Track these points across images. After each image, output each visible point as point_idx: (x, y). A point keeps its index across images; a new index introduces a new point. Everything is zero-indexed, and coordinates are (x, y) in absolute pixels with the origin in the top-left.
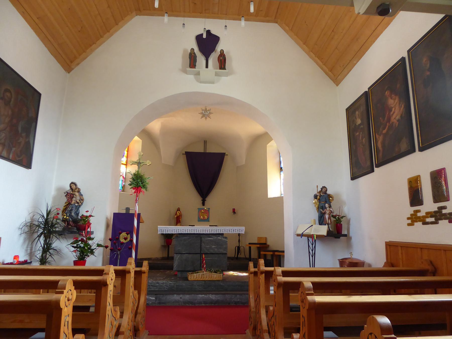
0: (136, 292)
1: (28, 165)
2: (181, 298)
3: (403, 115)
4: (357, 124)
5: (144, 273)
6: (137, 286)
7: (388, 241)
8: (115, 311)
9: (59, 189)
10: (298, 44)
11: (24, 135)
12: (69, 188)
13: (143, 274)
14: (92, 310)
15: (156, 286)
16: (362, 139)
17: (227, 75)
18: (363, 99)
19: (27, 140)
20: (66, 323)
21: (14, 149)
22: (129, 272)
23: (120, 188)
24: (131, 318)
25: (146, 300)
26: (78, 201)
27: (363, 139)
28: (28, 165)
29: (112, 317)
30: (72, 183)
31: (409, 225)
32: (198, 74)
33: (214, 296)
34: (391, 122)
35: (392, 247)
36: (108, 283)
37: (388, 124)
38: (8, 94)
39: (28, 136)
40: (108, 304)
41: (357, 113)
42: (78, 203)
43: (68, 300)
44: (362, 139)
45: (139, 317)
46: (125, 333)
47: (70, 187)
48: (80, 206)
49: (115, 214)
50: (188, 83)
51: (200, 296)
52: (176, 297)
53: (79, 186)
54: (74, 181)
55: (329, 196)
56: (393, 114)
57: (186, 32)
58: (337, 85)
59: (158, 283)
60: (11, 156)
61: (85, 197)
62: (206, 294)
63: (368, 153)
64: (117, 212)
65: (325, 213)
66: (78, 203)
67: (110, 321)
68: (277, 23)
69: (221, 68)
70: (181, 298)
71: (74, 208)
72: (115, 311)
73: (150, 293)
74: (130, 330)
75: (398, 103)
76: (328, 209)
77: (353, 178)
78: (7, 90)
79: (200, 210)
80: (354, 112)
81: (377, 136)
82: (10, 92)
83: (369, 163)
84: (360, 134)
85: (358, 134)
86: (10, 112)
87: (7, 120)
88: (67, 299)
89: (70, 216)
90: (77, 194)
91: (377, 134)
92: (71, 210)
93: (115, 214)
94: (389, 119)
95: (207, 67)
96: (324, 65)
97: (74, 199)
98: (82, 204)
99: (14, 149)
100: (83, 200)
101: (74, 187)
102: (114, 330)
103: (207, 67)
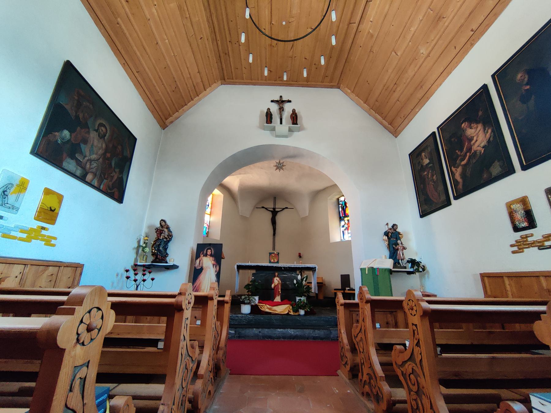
0: (219, 323)
1: (120, 199)
2: (260, 332)
3: (491, 139)
4: (425, 164)
5: (227, 303)
6: (219, 317)
7: (482, 272)
8: (192, 347)
9: (150, 227)
10: (358, 104)
11: (117, 170)
12: (159, 225)
13: (225, 304)
14: (161, 345)
15: (236, 320)
16: (432, 176)
17: (300, 130)
18: (432, 139)
19: (120, 176)
20: (77, 382)
21: (105, 181)
22: (212, 299)
23: (204, 233)
24: (212, 355)
25: (228, 333)
26: (166, 236)
27: (433, 176)
28: (120, 199)
29: (188, 358)
30: (162, 220)
31: (514, 252)
32: (273, 129)
33: (292, 330)
34: (473, 151)
35: (491, 280)
36: (184, 307)
37: (468, 154)
38: (103, 129)
39: (121, 172)
40: (182, 337)
41: (423, 154)
42: (166, 238)
43: (89, 329)
44: (432, 176)
45: (221, 353)
46: (204, 376)
47: (160, 224)
48: (169, 241)
49: (198, 245)
50: (264, 138)
51: (279, 330)
52: (255, 331)
53: (168, 223)
54: (164, 219)
55: (399, 233)
56: (474, 144)
57: (262, 97)
58: (396, 137)
59: (238, 317)
60: (102, 187)
61: (174, 234)
62: (285, 329)
63: (441, 188)
64: (202, 243)
65: (398, 249)
66: (166, 238)
67: (183, 365)
68: (339, 88)
69: (293, 124)
70: (260, 332)
71: (162, 243)
72: (192, 347)
73: (231, 326)
74: (211, 372)
75: (482, 130)
76: (400, 245)
77: (422, 216)
78: (101, 125)
79: (270, 254)
80: (419, 154)
81: (453, 169)
82: (104, 126)
83: (443, 198)
84: (428, 173)
85: (425, 173)
86: (104, 146)
87: (101, 152)
88: (83, 327)
89: (159, 250)
90: (166, 230)
91: (453, 168)
92: (160, 245)
93: (198, 245)
94: (470, 149)
95: (281, 123)
96: (384, 119)
97: (163, 234)
98: (170, 239)
99: (105, 181)
100: (171, 236)
101: (163, 224)
102: (191, 375)
103: (281, 123)
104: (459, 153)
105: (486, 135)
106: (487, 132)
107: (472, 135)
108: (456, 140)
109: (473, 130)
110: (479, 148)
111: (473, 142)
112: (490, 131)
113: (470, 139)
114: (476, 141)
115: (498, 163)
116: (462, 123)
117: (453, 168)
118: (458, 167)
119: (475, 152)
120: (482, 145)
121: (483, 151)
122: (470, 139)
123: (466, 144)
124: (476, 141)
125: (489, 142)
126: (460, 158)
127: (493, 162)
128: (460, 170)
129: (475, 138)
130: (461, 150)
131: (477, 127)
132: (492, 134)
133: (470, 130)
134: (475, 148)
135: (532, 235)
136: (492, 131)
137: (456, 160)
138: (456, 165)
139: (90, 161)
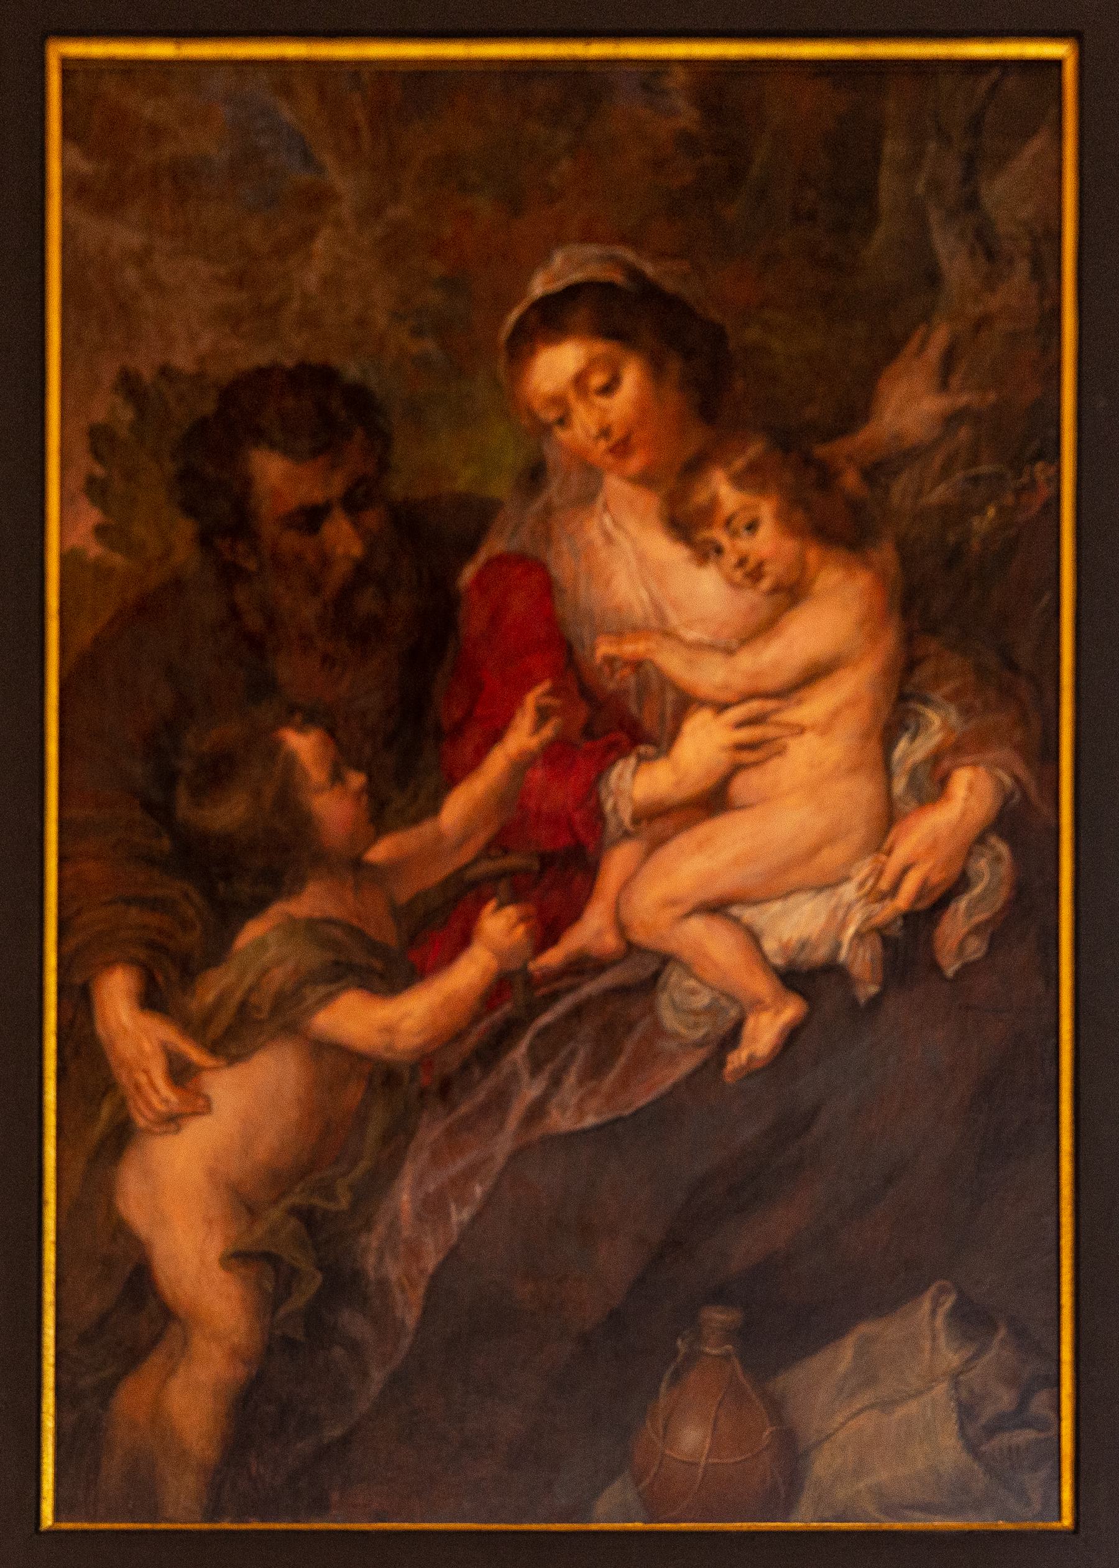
3: (957, 935)
34: (592, 930)
37: (499, 927)
56: (665, 820)
75: (850, 692)
91: (117, 996)
94: (553, 856)
104: (333, 808)
105: (889, 818)
106: (932, 784)
107: (672, 662)
108: (343, 539)
109: (704, 594)
110: (714, 945)
111: (637, 783)
112: (970, 794)
113: (620, 718)
114: (714, 800)
115: (951, 1357)
116: (550, 319)
117: (117, 996)
118: (232, 1036)
119: (646, 970)
120: (797, 923)
121: (764, 1033)
122: (620, 718)
123: (522, 737)
124: (714, 800)
125: (907, 940)
126: (312, 901)
127: (886, 1304)
128: (248, 1103)
129: (702, 744)
130: (408, 757)
131: (792, 593)
132: (992, 873)
133: (664, 549)
134: (651, 891)
135: (740, 725)
136: (1017, 824)
137: (232, 876)
138: (214, 987)
139: (311, 518)
